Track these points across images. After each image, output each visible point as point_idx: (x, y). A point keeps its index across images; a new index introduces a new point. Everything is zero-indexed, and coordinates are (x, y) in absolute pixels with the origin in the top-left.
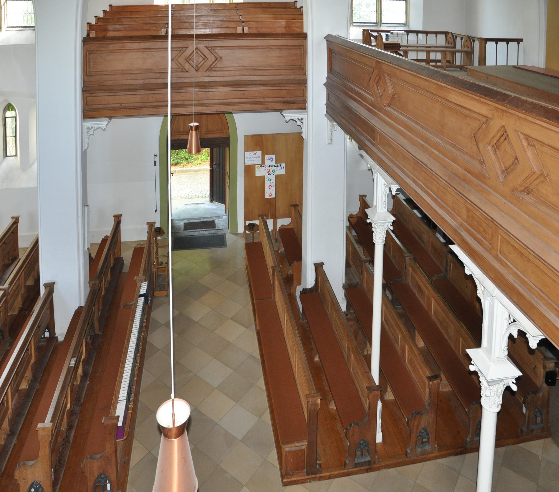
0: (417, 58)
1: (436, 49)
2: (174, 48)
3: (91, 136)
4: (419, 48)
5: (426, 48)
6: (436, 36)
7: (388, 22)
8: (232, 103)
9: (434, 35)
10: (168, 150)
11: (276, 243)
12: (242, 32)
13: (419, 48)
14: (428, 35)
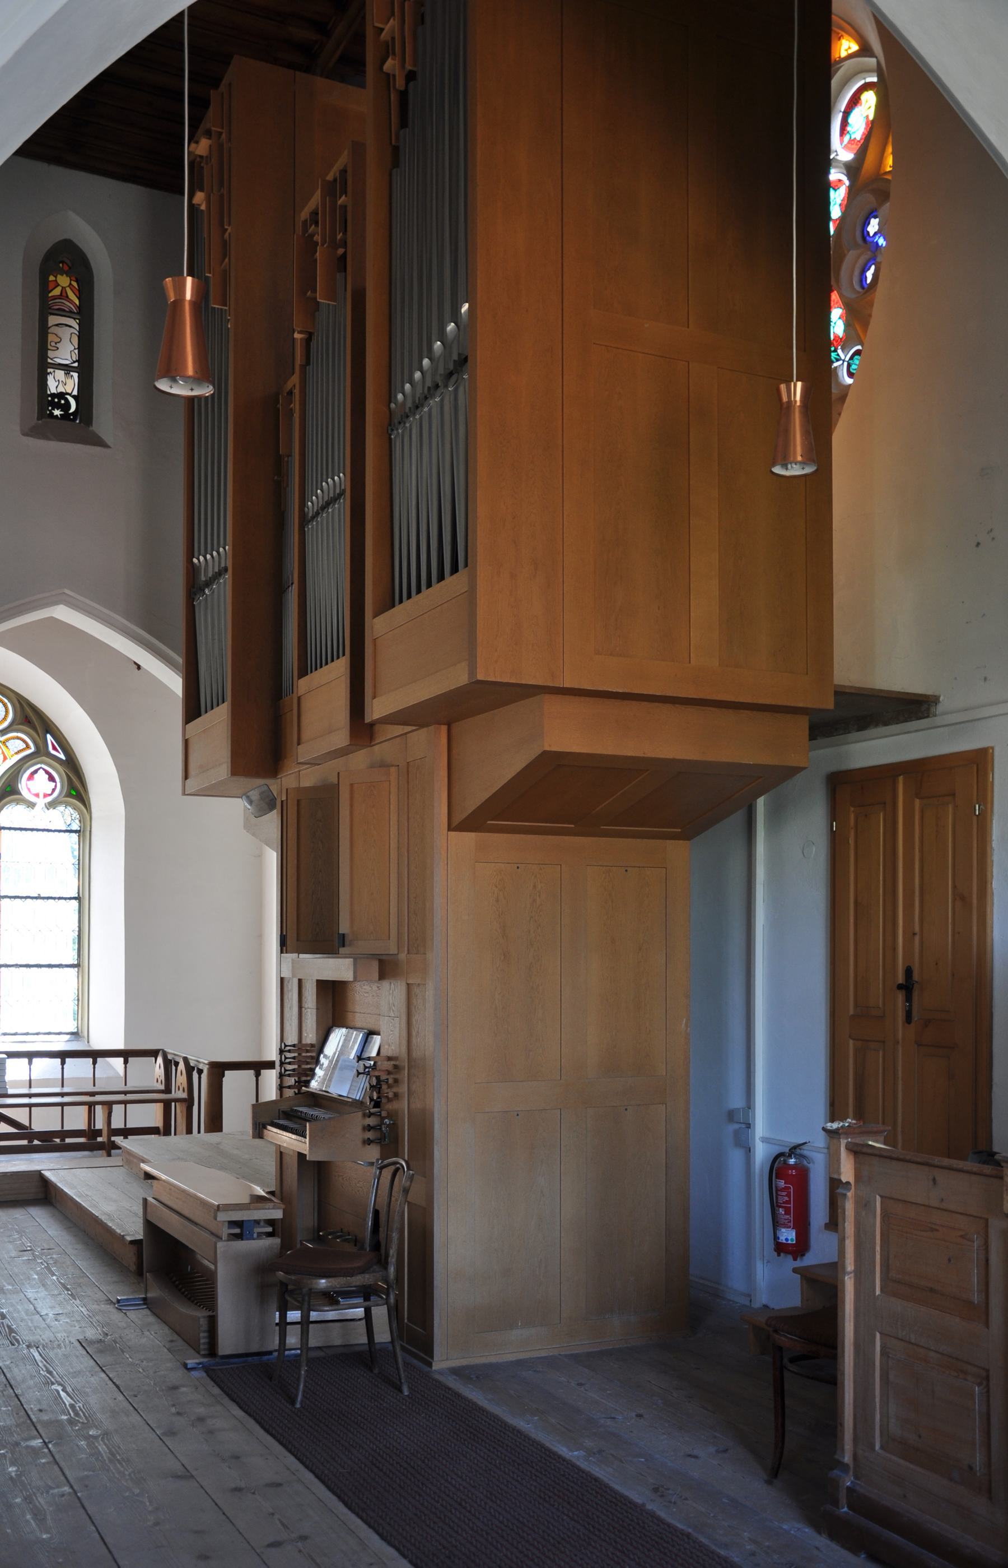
0: (125, 1125)
1: (131, 1097)
2: (279, 1116)
3: (50, 793)
4: (130, 1097)
5: (91, 1096)
6: (95, 1063)
7: (53, 963)
8: (346, 184)
9: (26, 1060)
10: (193, 468)
11: (372, 1371)
12: (289, 1320)
13: (130, 1097)
14: (130, 1059)
